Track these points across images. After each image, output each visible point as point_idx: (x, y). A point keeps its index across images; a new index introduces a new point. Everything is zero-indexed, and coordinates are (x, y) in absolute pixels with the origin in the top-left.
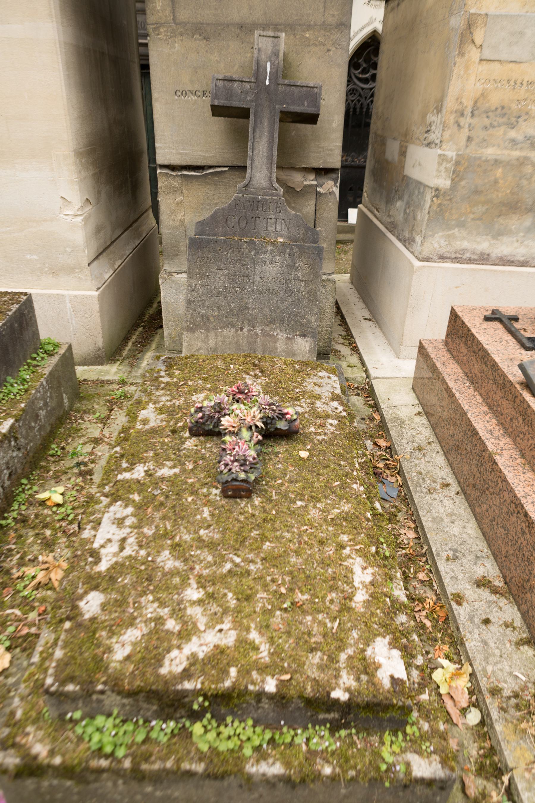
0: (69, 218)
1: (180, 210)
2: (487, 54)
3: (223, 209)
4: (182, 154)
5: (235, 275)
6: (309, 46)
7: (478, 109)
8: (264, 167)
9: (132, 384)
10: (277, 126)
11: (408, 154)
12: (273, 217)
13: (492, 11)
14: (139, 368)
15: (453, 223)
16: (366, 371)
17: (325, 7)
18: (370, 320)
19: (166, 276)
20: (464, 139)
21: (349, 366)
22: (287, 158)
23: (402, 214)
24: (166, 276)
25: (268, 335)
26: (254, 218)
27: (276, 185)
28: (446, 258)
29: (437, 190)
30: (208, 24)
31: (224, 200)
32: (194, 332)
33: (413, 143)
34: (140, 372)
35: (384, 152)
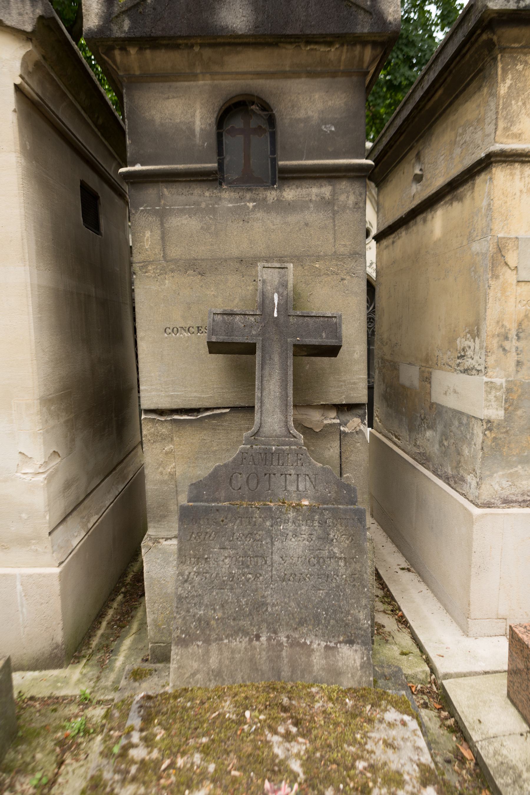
0: (28, 477)
1: (169, 463)
2: (524, 275)
3: (225, 466)
4: (172, 396)
5: (246, 555)
6: (320, 276)
7: (523, 331)
8: (277, 410)
9: (99, 702)
10: (290, 362)
11: (434, 380)
12: (293, 472)
13: (521, 234)
14: (112, 670)
15: (514, 459)
16: (428, 661)
17: (335, 238)
18: (409, 570)
19: (151, 544)
20: (513, 364)
21: (403, 654)
22: (303, 395)
23: (437, 446)
24: (151, 544)
25: (298, 644)
26: (269, 475)
27: (294, 431)
28: (512, 502)
29: (489, 421)
30: (203, 260)
31: (224, 447)
32: (187, 646)
33: (440, 369)
34: (112, 677)
35: (398, 377)
